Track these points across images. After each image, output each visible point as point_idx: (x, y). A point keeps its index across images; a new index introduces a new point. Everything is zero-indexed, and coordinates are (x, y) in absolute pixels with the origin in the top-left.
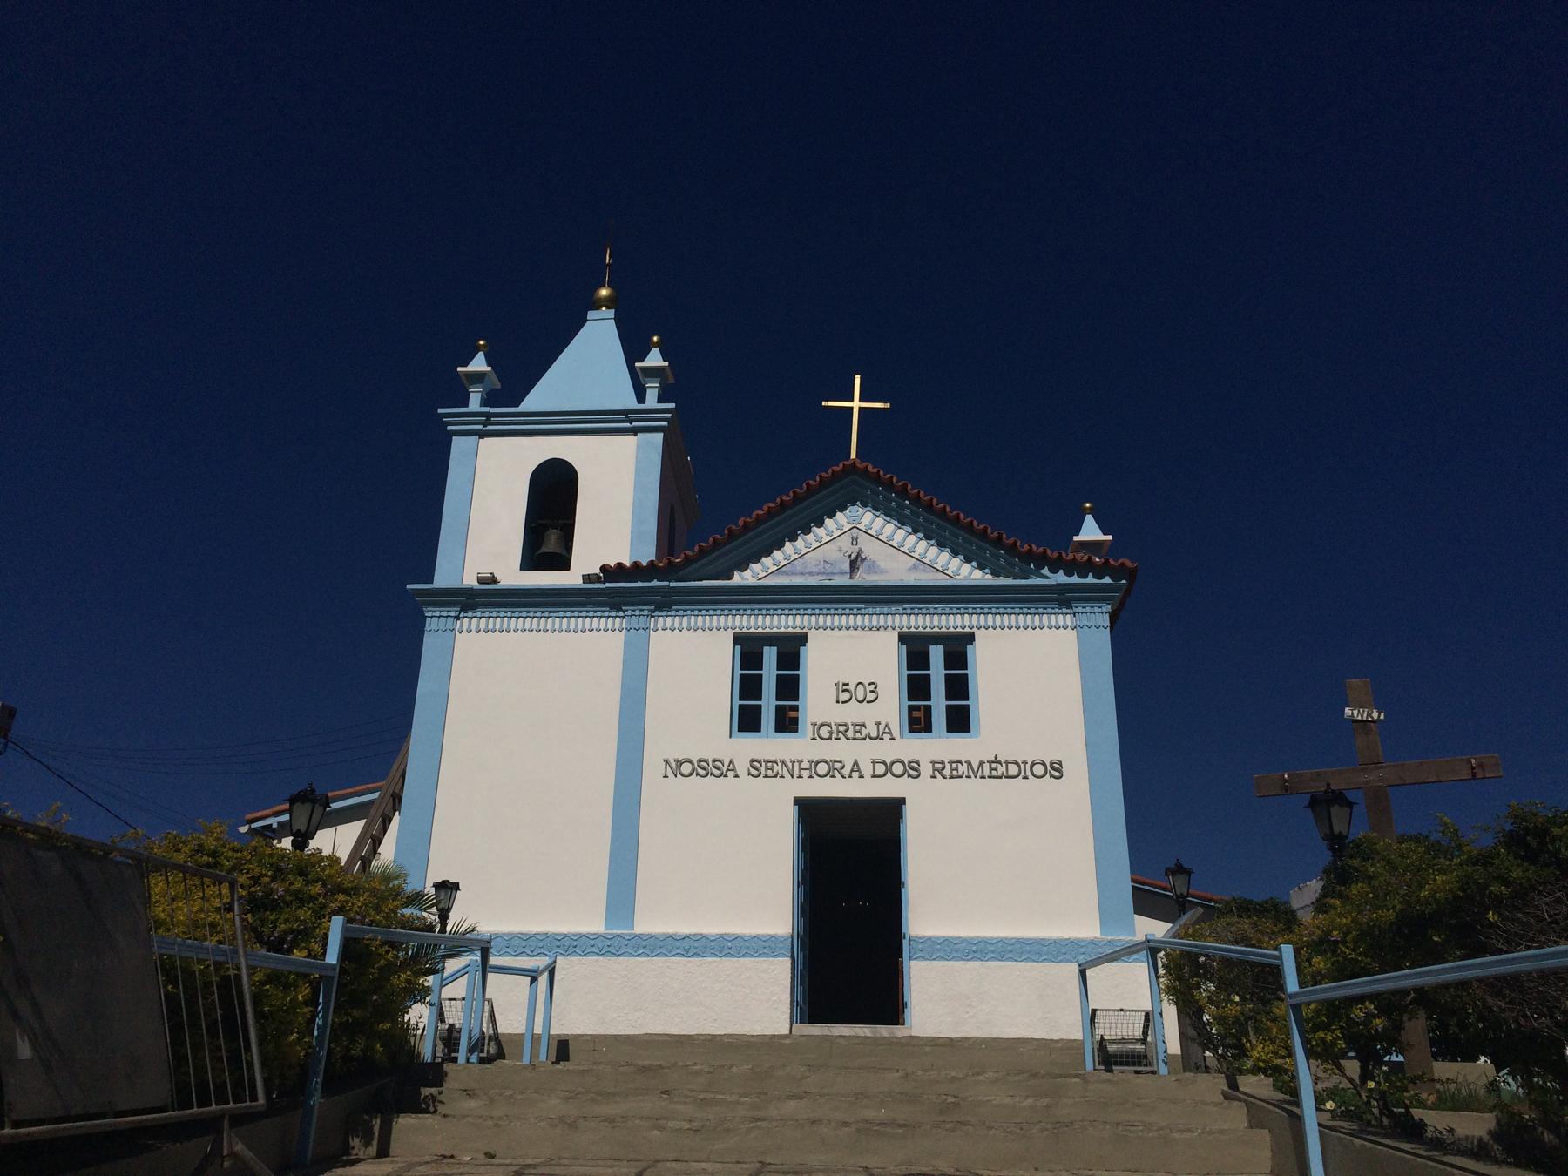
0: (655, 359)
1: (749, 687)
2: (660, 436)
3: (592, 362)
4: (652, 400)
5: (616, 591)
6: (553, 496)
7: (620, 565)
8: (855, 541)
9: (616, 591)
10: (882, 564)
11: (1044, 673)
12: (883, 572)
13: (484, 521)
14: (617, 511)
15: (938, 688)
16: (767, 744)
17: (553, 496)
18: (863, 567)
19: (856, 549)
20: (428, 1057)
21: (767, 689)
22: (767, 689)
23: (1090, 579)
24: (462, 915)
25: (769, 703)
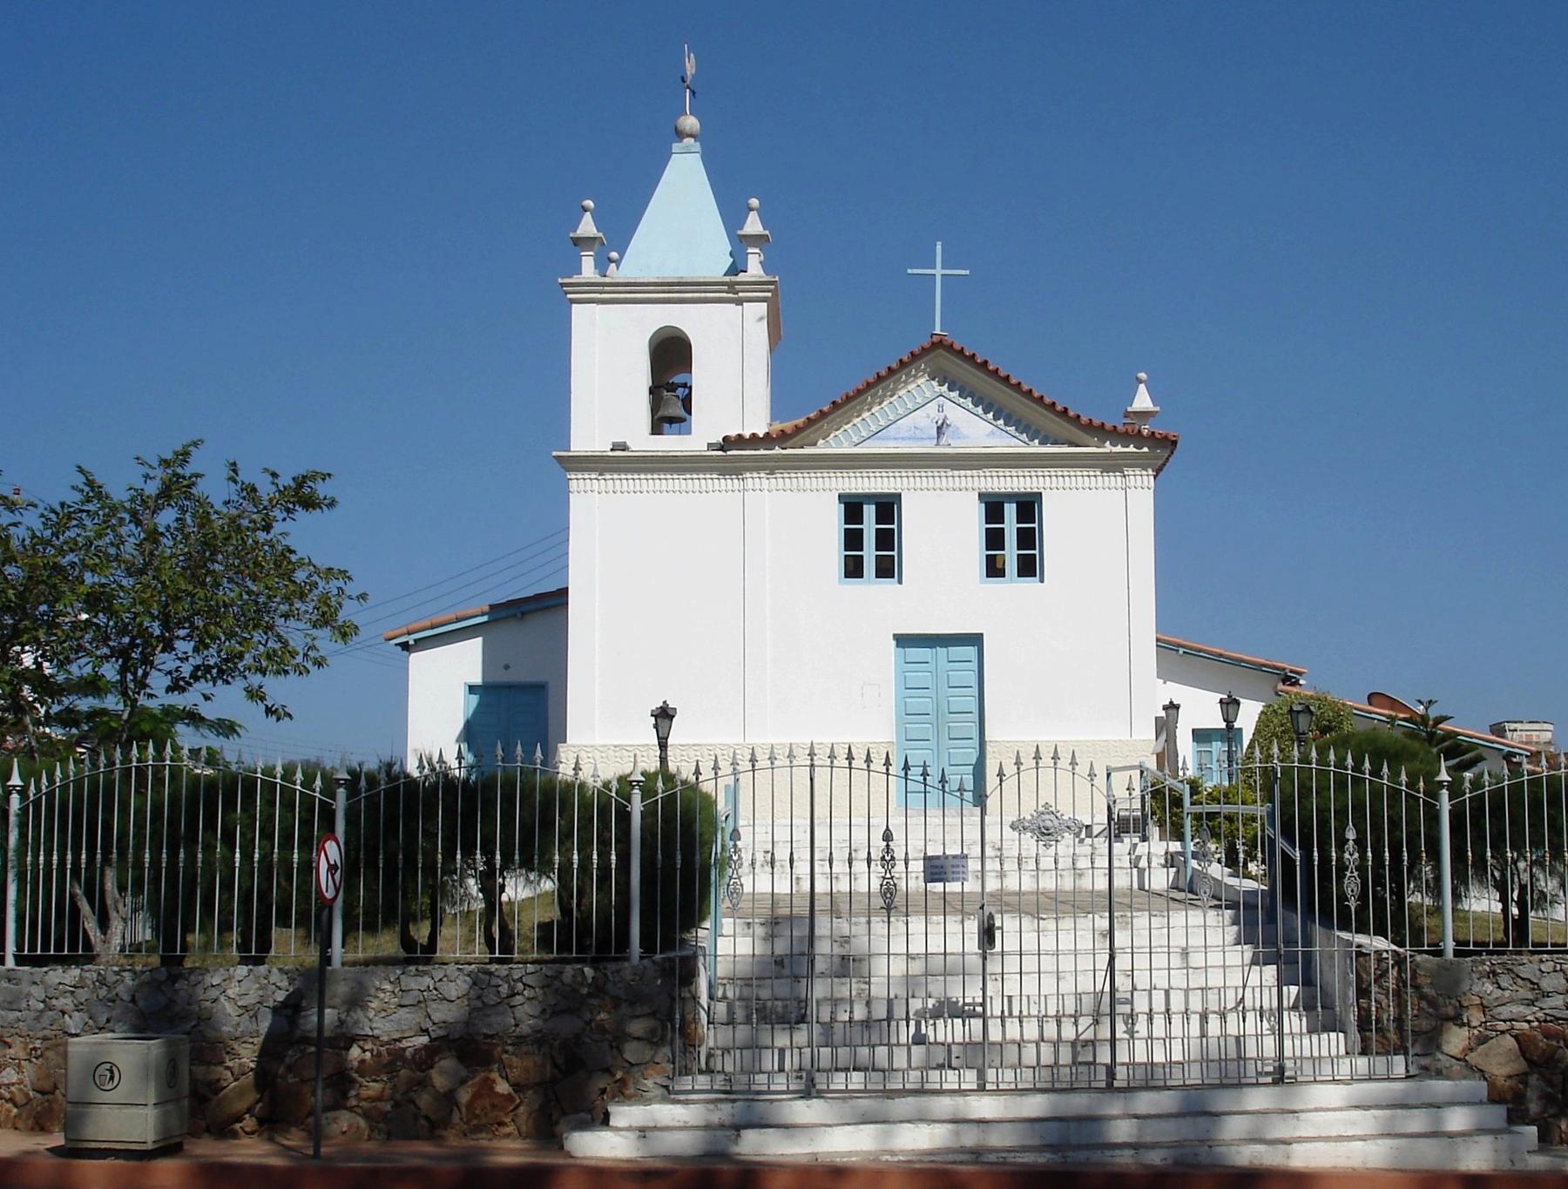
0: (753, 225)
3: (683, 219)
5: (734, 457)
6: (670, 357)
8: (941, 408)
9: (734, 457)
10: (964, 431)
11: (1103, 521)
12: (966, 437)
14: (735, 384)
15: (1013, 538)
16: (870, 588)
17: (670, 357)
18: (948, 432)
20: (416, 774)
21: (873, 538)
22: (873, 538)
23: (1132, 449)
25: (869, 553)
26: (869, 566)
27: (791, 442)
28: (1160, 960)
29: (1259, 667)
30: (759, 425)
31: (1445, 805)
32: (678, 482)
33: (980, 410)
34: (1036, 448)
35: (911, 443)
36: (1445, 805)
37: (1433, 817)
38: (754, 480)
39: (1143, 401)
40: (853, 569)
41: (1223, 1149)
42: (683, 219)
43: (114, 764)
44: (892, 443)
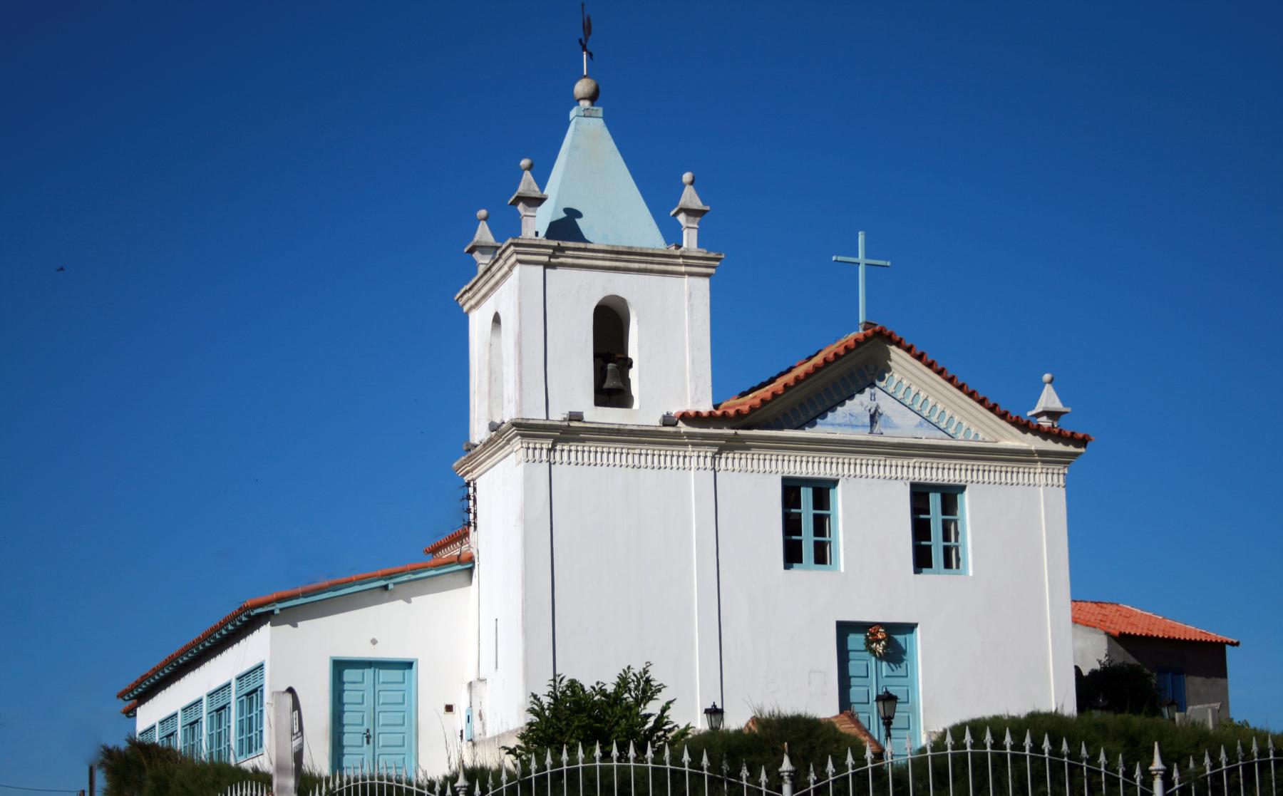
1: (791, 526)
2: (706, 282)
3: (588, 169)
4: (690, 240)
6: (610, 325)
7: (697, 413)
10: (896, 420)
12: (896, 427)
13: (518, 342)
14: (676, 361)
15: (932, 531)
16: (807, 573)
17: (610, 325)
18: (880, 422)
19: (874, 404)
21: (805, 527)
22: (805, 527)
24: (610, 688)
26: (808, 551)
30: (706, 407)
35: (849, 430)
40: (792, 555)
42: (588, 169)
43: (865, 762)
44: (830, 429)
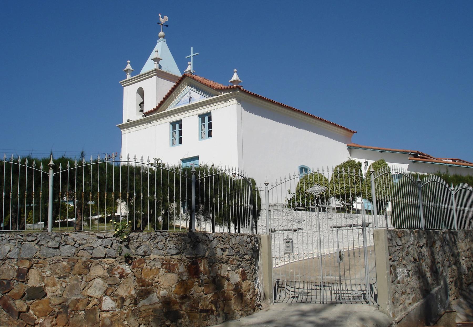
10: (195, 98)
16: (178, 147)
18: (192, 99)
23: (228, 93)
27: (158, 111)
28: (310, 247)
29: (402, 152)
31: (51, 174)
32: (140, 127)
33: (198, 92)
34: (210, 98)
36: (51, 174)
37: (46, 177)
38: (154, 123)
39: (235, 77)
41: (412, 317)
